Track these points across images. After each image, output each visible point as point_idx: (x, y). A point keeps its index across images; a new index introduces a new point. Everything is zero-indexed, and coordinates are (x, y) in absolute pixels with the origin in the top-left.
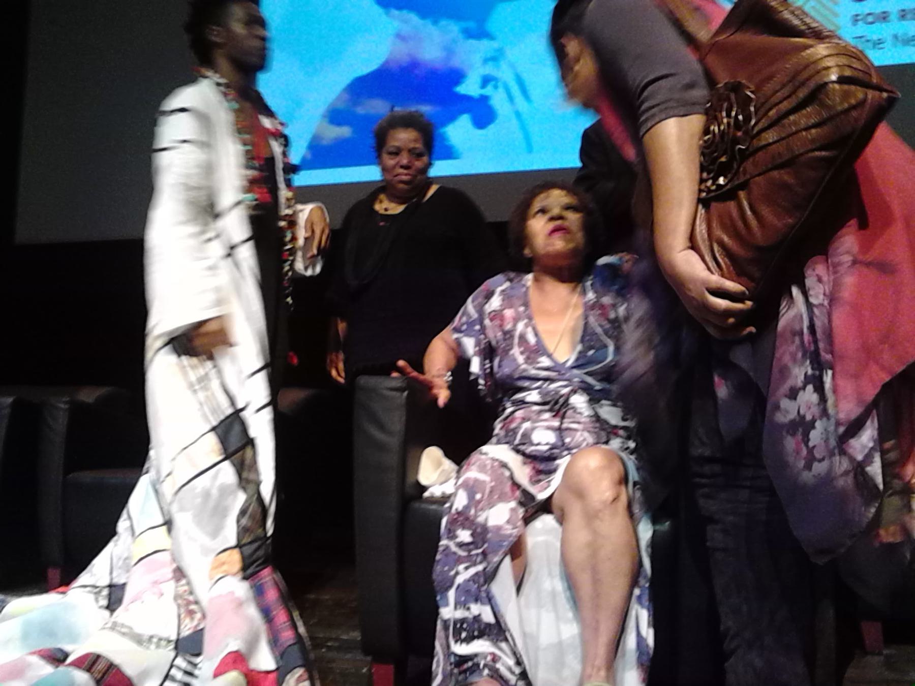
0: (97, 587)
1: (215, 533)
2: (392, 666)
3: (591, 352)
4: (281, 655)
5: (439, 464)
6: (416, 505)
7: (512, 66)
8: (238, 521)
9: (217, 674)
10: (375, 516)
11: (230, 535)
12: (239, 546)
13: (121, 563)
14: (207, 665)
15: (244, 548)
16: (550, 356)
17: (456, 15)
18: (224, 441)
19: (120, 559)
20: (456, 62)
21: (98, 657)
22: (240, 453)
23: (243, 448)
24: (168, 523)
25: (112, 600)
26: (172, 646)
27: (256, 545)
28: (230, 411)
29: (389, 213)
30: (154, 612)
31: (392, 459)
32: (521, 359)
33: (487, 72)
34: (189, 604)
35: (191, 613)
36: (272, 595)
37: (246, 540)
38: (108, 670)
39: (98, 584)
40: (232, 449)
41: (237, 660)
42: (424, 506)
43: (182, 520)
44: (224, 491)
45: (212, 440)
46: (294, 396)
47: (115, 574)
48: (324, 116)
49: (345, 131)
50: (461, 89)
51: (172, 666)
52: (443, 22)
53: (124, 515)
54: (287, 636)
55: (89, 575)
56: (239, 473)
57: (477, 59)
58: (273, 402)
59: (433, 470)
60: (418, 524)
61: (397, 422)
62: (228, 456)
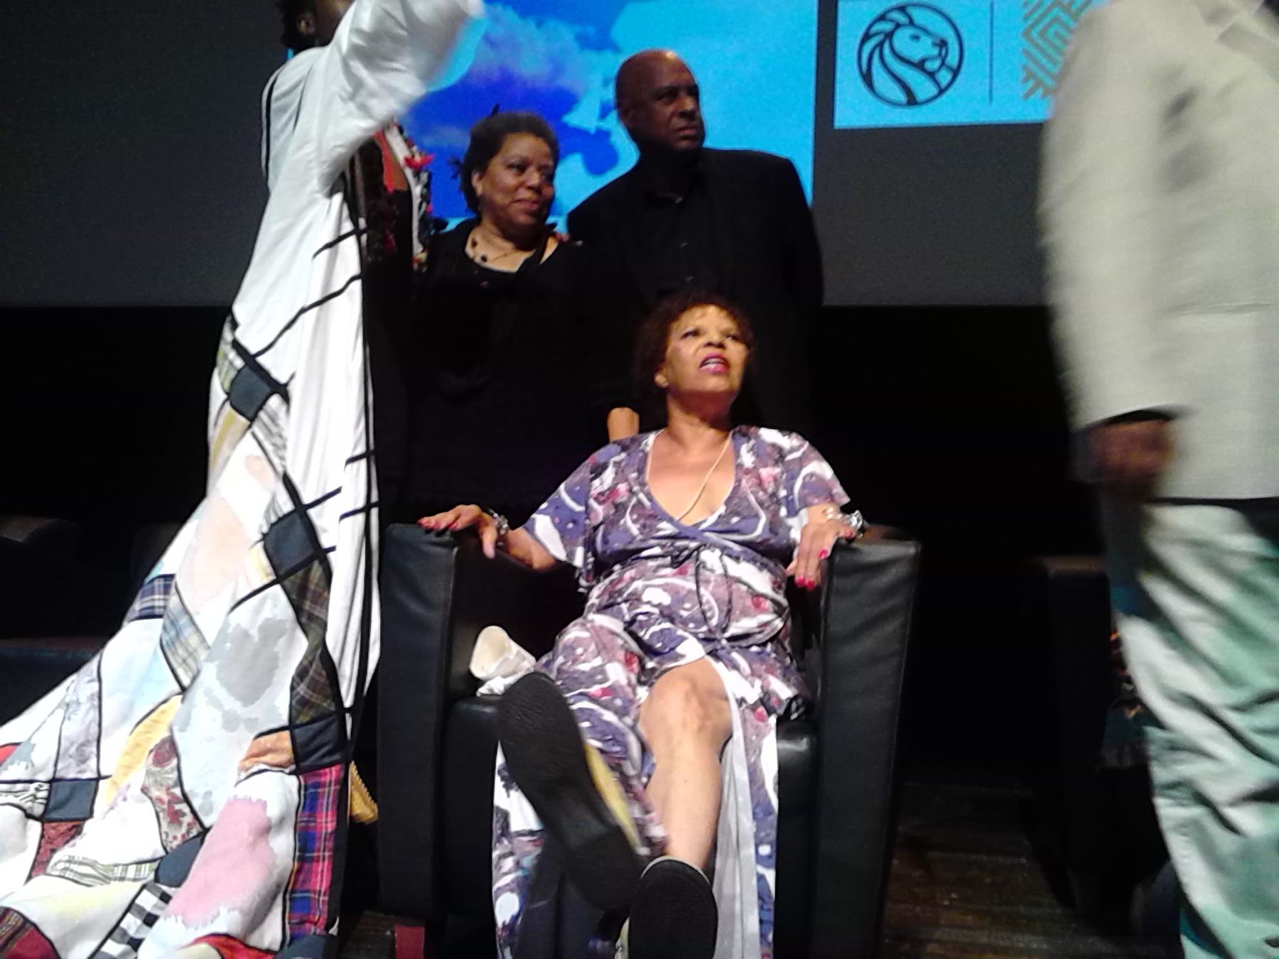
2: (423, 929)
3: (735, 520)
5: (503, 650)
6: (464, 706)
8: (292, 688)
11: (278, 706)
12: (291, 727)
13: (73, 750)
15: (297, 731)
16: (671, 520)
17: (573, 15)
19: (72, 744)
20: (565, 81)
22: (300, 573)
27: (317, 726)
28: (286, 506)
29: (489, 265)
31: (433, 641)
32: (635, 529)
37: (303, 719)
42: (476, 708)
44: (270, 631)
47: (60, 766)
50: (574, 119)
52: (551, 24)
56: (298, 609)
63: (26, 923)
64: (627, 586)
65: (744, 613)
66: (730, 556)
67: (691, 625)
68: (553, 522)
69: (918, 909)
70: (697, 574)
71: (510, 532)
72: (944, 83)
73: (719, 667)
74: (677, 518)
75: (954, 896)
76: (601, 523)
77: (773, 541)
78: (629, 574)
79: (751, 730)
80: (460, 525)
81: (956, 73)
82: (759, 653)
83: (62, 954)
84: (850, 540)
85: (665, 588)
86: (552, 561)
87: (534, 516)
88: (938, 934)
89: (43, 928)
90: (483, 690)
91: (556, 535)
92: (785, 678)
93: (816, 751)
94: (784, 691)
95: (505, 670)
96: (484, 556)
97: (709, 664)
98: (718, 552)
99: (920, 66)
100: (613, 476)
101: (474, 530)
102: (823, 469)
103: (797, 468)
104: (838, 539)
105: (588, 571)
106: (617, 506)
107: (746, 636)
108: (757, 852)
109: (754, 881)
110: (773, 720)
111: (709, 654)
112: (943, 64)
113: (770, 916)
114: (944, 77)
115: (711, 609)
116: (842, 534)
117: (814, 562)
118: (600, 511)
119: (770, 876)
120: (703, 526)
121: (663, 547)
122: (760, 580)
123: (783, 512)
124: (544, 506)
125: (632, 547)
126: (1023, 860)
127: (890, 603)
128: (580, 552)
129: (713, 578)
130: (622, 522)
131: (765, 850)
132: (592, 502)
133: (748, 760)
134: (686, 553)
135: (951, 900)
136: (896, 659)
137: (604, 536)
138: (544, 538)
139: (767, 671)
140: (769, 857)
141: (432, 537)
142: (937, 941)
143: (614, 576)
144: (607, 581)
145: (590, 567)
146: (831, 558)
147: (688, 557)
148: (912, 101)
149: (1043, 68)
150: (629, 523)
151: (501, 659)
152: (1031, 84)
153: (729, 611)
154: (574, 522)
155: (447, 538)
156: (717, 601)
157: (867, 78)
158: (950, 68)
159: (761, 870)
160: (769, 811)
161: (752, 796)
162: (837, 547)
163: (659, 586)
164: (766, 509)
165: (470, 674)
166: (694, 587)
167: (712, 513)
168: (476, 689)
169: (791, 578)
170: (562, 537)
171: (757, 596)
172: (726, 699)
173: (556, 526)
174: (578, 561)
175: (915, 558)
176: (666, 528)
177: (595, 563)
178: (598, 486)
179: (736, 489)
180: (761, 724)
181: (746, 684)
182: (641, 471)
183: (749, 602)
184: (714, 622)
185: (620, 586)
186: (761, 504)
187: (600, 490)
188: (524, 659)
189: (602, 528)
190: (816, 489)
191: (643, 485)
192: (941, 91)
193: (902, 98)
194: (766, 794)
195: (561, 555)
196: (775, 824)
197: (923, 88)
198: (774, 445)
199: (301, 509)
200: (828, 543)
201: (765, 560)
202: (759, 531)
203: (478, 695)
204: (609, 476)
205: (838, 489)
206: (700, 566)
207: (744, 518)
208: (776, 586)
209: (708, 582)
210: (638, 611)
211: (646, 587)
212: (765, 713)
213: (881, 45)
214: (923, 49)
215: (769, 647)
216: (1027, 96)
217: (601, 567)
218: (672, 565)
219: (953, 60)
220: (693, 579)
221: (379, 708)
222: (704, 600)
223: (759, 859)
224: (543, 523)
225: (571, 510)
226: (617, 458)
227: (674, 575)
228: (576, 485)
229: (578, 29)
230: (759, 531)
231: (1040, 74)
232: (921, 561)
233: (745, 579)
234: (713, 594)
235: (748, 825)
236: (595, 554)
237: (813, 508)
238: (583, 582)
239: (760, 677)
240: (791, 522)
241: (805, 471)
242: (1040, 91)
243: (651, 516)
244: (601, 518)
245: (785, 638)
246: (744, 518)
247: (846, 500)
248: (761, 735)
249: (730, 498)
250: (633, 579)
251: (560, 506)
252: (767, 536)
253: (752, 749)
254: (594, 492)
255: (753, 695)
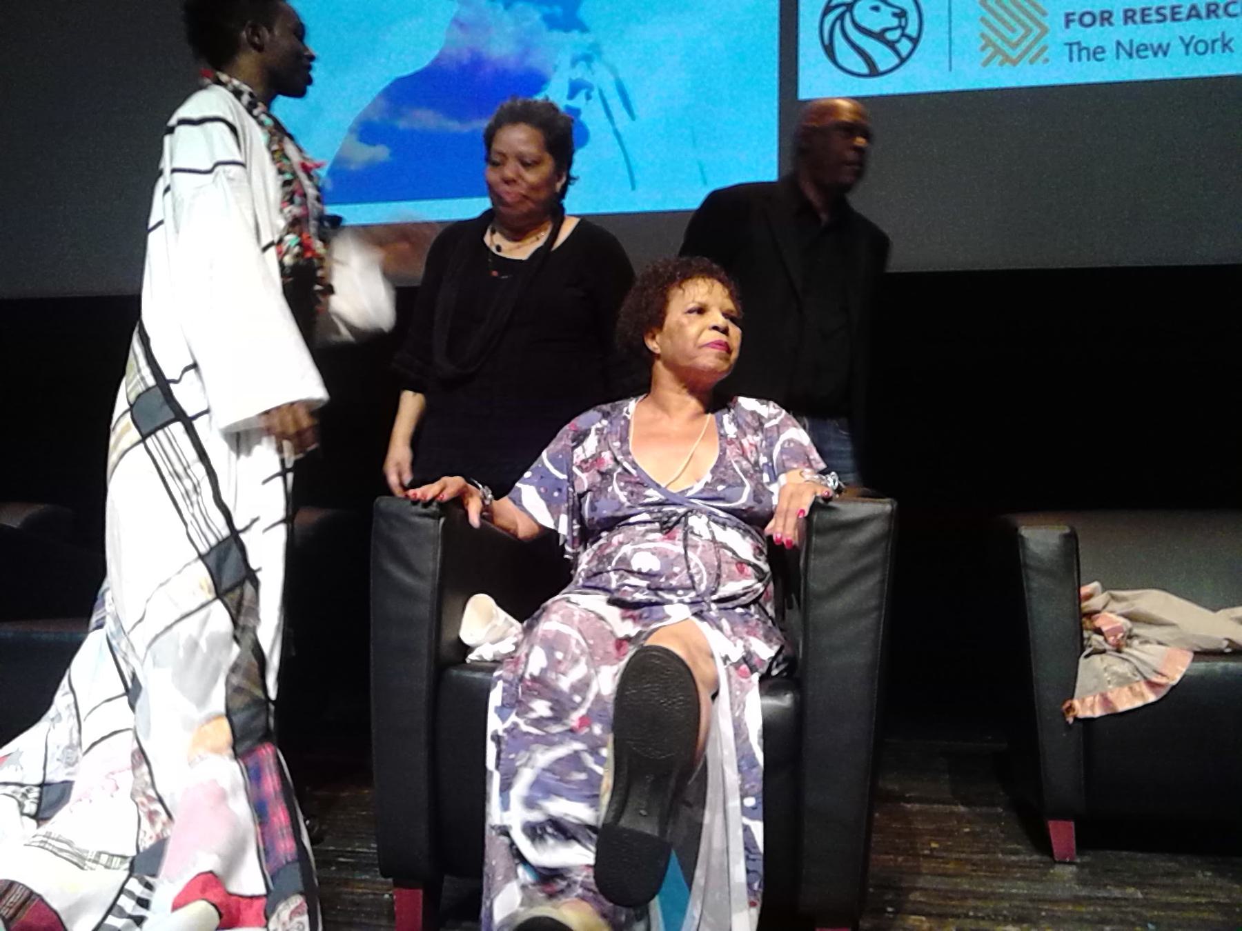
0: (22, 785)
1: (202, 701)
3: (720, 488)
4: (273, 876)
7: (613, 71)
9: (176, 907)
10: (400, 688)
14: (167, 888)
18: (216, 575)
20: (534, 61)
21: (11, 884)
23: (240, 584)
24: (133, 691)
25: (43, 805)
26: (127, 865)
30: (103, 819)
31: (424, 610)
32: (622, 496)
33: (579, 76)
34: (155, 805)
35: (152, 815)
36: (271, 783)
38: (24, 903)
39: (25, 782)
40: (226, 583)
41: (208, 884)
42: (468, 674)
43: (154, 682)
45: (201, 574)
46: (309, 517)
48: (351, 130)
49: (381, 153)
51: (122, 891)
53: (65, 681)
54: (285, 847)
55: (13, 767)
57: (564, 59)
58: (288, 520)
59: (483, 625)
60: (457, 695)
61: (429, 559)
62: (220, 593)
63: (31, 896)
64: (616, 552)
65: (731, 578)
66: (716, 522)
67: (680, 592)
68: (539, 493)
69: (900, 859)
70: (685, 539)
71: (494, 502)
72: (904, 53)
73: (704, 626)
74: (663, 485)
75: (934, 845)
76: (588, 490)
77: (756, 509)
78: (616, 539)
79: (735, 686)
80: (446, 496)
81: (915, 41)
82: (742, 615)
83: (68, 926)
84: (827, 499)
85: (654, 552)
86: (536, 529)
87: (518, 485)
88: (921, 883)
89: (48, 899)
90: (472, 657)
91: (543, 504)
92: (768, 639)
93: (800, 708)
94: (765, 651)
95: (493, 637)
96: (471, 527)
97: (694, 624)
98: (705, 519)
99: (880, 36)
100: (596, 444)
101: (459, 501)
102: (798, 434)
103: (775, 434)
104: (816, 498)
105: (574, 538)
106: (601, 474)
107: (732, 598)
108: (742, 804)
109: (740, 832)
110: (755, 677)
111: (695, 614)
112: (903, 35)
113: (759, 866)
114: (905, 47)
115: (699, 572)
116: (819, 494)
117: (792, 521)
118: (584, 480)
119: (758, 828)
120: (690, 494)
121: (650, 513)
122: (744, 547)
123: (766, 478)
124: (527, 475)
125: (620, 514)
126: (1000, 810)
127: (867, 560)
128: (564, 519)
129: (700, 543)
130: (610, 489)
131: (750, 802)
132: (575, 469)
133: (733, 714)
134: (674, 519)
135: (932, 850)
136: (874, 615)
137: (592, 502)
138: (531, 507)
139: (748, 633)
140: (754, 808)
141: (419, 509)
142: (921, 889)
143: (601, 542)
144: (595, 546)
145: (575, 534)
146: (808, 519)
147: (678, 522)
148: (874, 72)
149: (1002, 37)
150: (617, 490)
151: (489, 626)
152: (990, 50)
153: (719, 576)
154: (560, 490)
155: (434, 508)
156: (707, 568)
157: (829, 50)
158: (910, 38)
159: (746, 821)
160: (754, 764)
161: (737, 749)
162: (815, 506)
163: (647, 550)
164: (750, 478)
165: (459, 640)
166: (683, 552)
167: (698, 481)
168: (466, 656)
169: (770, 537)
170: (548, 506)
171: (741, 563)
172: (712, 656)
173: (541, 495)
174: (563, 530)
175: (891, 516)
176: (654, 495)
177: (581, 531)
178: (579, 454)
179: (721, 458)
180: (744, 680)
181: (729, 644)
182: (624, 440)
183: (734, 568)
184: (703, 588)
185: (608, 551)
186: (745, 472)
187: (583, 457)
188: (512, 625)
189: (589, 495)
190: (796, 453)
191: (627, 453)
192: (903, 61)
193: (864, 69)
194: (750, 746)
195: (549, 524)
196: (761, 776)
197: (883, 56)
198: (753, 413)
199: (235, 534)
200: (806, 503)
201: (748, 527)
202: (744, 499)
203: (468, 661)
204: (591, 444)
205: (815, 455)
206: (688, 531)
207: (729, 486)
208: (758, 551)
209: (696, 547)
210: (626, 582)
211: (635, 551)
212: (748, 670)
213: (841, 17)
214: (883, 19)
215: (753, 609)
216: (987, 62)
217: (587, 534)
218: (661, 530)
219: (912, 30)
220: (681, 543)
221: (372, 675)
222: (692, 565)
223: (745, 811)
224: (528, 493)
225: (557, 479)
226: (599, 425)
227: (663, 540)
228: (558, 452)
229: (546, 10)
230: (744, 499)
231: (999, 42)
232: (897, 518)
233: (730, 545)
234: (700, 558)
235: (732, 777)
236: (581, 520)
237: (791, 473)
238: (568, 549)
239: (742, 638)
240: (774, 488)
241: (783, 438)
242: (999, 58)
243: (638, 483)
244: (586, 487)
245: (766, 601)
246: (729, 486)
247: (822, 466)
248: (744, 690)
249: (716, 467)
250: (621, 544)
251: (544, 475)
252: (752, 503)
253: (737, 704)
254: (576, 460)
255: (736, 654)
